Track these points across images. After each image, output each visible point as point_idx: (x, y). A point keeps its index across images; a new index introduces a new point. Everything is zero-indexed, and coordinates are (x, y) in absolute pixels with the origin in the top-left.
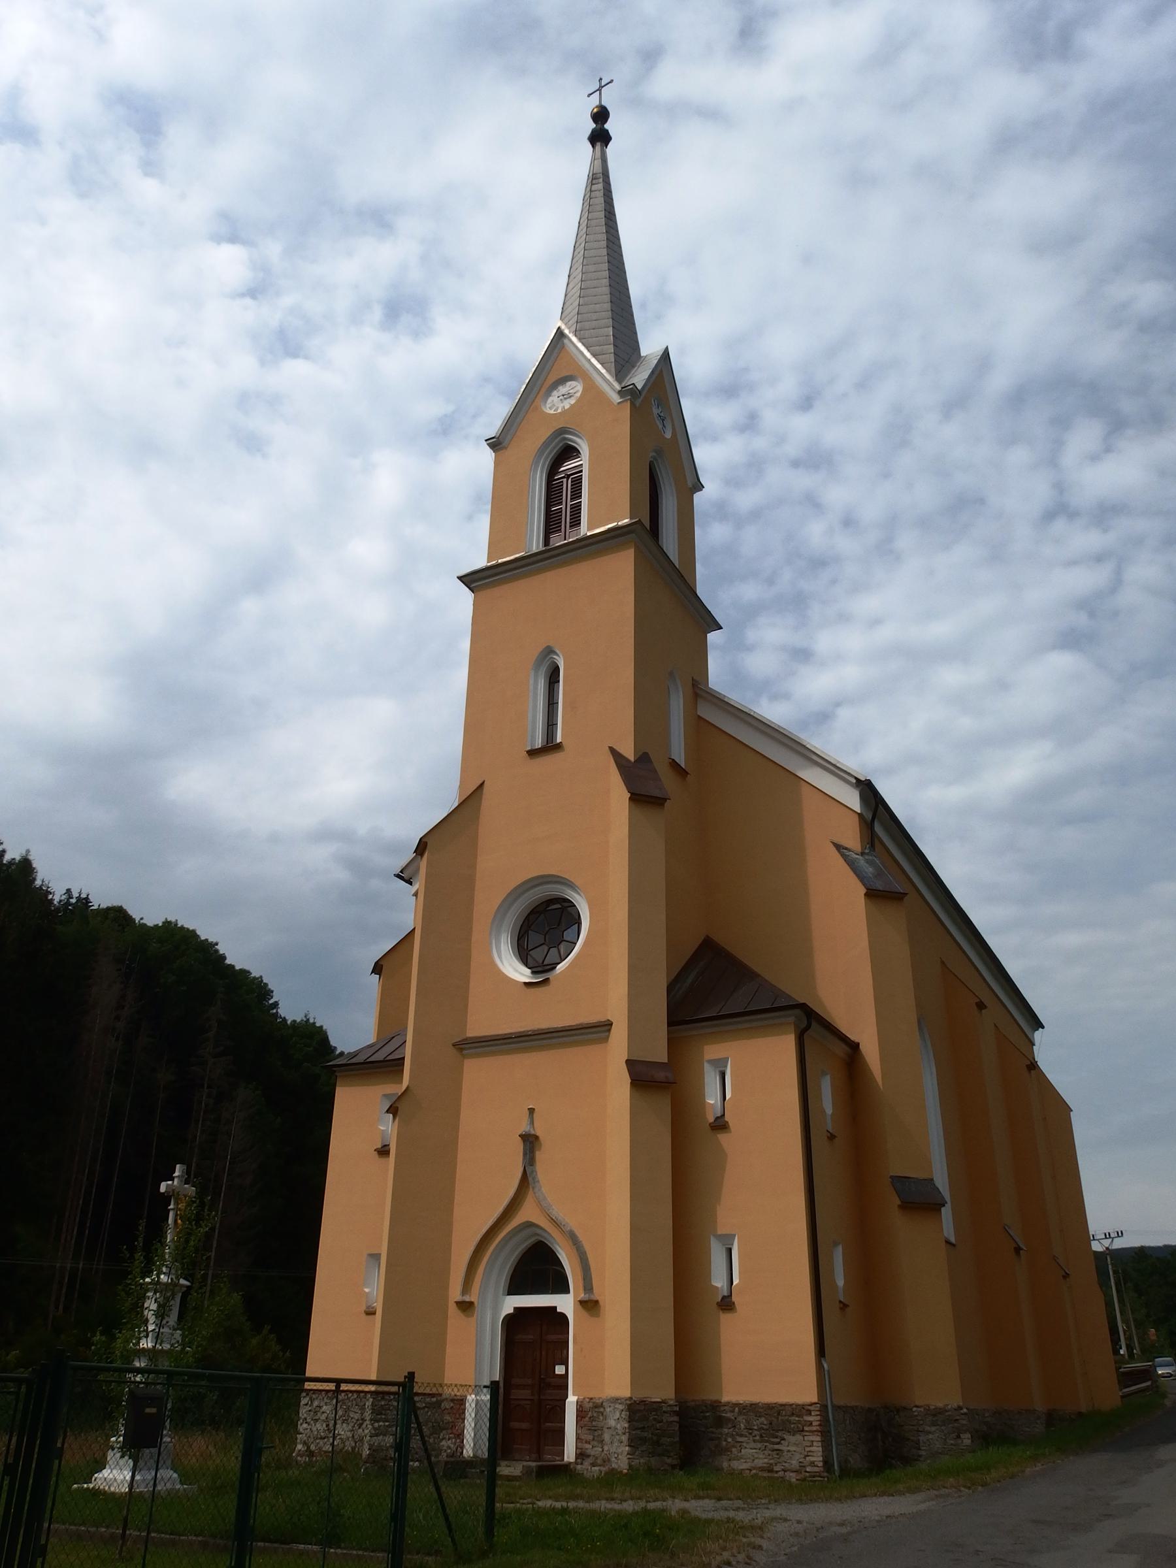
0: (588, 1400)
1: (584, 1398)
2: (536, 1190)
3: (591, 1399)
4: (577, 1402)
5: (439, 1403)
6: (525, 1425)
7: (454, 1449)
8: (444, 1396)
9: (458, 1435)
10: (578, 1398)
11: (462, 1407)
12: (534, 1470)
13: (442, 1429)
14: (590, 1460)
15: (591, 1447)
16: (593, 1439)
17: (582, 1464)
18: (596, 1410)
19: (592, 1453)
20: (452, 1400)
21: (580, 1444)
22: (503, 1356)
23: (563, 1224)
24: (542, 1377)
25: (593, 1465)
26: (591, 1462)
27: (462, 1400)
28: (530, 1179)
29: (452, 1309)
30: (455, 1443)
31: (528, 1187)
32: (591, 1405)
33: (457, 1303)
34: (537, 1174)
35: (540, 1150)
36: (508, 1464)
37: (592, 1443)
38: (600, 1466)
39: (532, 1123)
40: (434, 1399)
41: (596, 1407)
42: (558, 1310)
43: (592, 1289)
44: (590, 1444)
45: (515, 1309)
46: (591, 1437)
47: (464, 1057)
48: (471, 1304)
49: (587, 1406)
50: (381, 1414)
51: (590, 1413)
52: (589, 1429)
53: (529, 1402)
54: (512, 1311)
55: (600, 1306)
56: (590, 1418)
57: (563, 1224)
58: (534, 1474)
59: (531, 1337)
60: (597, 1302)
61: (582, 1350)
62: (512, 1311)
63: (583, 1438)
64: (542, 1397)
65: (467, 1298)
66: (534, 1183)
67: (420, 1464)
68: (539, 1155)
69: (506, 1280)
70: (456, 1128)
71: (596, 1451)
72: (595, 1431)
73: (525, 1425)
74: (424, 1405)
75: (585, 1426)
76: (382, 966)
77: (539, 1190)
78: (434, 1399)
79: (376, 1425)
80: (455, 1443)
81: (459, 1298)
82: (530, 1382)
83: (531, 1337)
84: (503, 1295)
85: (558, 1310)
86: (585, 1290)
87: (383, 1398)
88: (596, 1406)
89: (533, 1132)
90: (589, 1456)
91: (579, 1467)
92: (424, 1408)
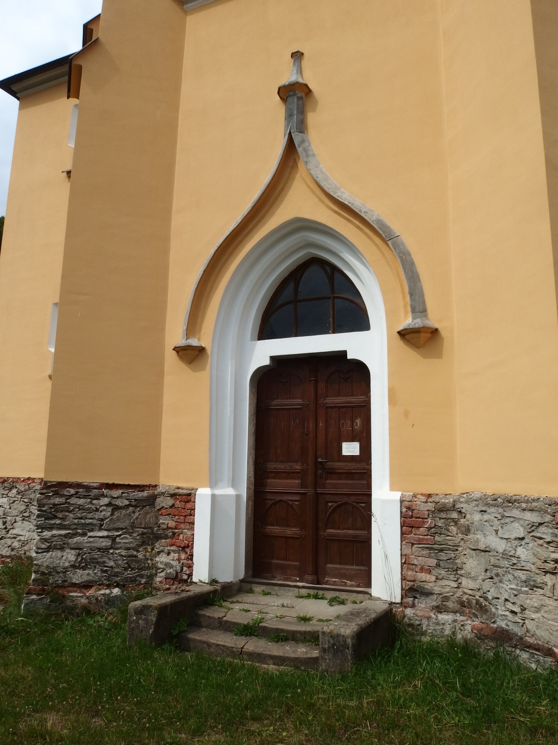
0: (423, 499)
1: (415, 496)
2: (310, 166)
3: (429, 496)
4: (402, 501)
5: (151, 500)
6: (290, 531)
7: (179, 568)
8: (160, 489)
9: (184, 548)
10: (402, 496)
11: (189, 505)
12: (349, 641)
13: (158, 537)
14: (433, 601)
15: (433, 578)
16: (438, 565)
17: (413, 606)
18: (443, 515)
19: (437, 590)
20: (173, 496)
21: (410, 573)
22: (253, 430)
23: (363, 210)
24: (320, 460)
25: (439, 609)
26: (435, 604)
27: (190, 495)
28: (300, 150)
29: (171, 357)
30: (179, 560)
31: (295, 166)
32: (431, 506)
33: (178, 350)
34: (310, 145)
35: (314, 110)
36: (266, 591)
37: (435, 572)
38: (455, 612)
39: (300, 71)
40: (145, 494)
41: (441, 510)
42: (349, 357)
43: (424, 311)
44: (430, 572)
45: (272, 358)
46: (433, 562)
47: (186, 12)
48: (201, 350)
49: (423, 508)
50: (55, 517)
51: (429, 520)
52: (430, 549)
53: (297, 498)
54: (267, 362)
55: (442, 339)
56: (429, 528)
57: (363, 210)
58: (349, 652)
59: (300, 401)
60: (435, 332)
61: (406, 414)
62: (267, 362)
63: (415, 562)
64: (319, 490)
65: (194, 342)
66: (307, 156)
67: (122, 591)
68: (312, 118)
69: (253, 326)
70: (175, 107)
71: (443, 587)
72: (441, 550)
73: (290, 531)
74: (127, 502)
75: (420, 541)
76: (92, 30)
77: (317, 167)
78: (145, 494)
79: (47, 534)
80: (179, 560)
81: (181, 342)
82: (298, 467)
83: (300, 401)
84: (252, 340)
85: (349, 357)
86: (413, 311)
87: (56, 494)
88: (442, 509)
89: (300, 80)
90: (428, 594)
91: (409, 612)
92: (127, 506)
